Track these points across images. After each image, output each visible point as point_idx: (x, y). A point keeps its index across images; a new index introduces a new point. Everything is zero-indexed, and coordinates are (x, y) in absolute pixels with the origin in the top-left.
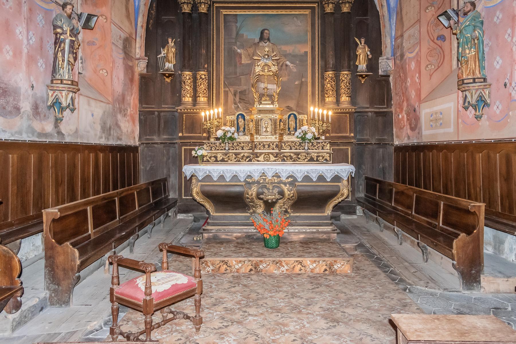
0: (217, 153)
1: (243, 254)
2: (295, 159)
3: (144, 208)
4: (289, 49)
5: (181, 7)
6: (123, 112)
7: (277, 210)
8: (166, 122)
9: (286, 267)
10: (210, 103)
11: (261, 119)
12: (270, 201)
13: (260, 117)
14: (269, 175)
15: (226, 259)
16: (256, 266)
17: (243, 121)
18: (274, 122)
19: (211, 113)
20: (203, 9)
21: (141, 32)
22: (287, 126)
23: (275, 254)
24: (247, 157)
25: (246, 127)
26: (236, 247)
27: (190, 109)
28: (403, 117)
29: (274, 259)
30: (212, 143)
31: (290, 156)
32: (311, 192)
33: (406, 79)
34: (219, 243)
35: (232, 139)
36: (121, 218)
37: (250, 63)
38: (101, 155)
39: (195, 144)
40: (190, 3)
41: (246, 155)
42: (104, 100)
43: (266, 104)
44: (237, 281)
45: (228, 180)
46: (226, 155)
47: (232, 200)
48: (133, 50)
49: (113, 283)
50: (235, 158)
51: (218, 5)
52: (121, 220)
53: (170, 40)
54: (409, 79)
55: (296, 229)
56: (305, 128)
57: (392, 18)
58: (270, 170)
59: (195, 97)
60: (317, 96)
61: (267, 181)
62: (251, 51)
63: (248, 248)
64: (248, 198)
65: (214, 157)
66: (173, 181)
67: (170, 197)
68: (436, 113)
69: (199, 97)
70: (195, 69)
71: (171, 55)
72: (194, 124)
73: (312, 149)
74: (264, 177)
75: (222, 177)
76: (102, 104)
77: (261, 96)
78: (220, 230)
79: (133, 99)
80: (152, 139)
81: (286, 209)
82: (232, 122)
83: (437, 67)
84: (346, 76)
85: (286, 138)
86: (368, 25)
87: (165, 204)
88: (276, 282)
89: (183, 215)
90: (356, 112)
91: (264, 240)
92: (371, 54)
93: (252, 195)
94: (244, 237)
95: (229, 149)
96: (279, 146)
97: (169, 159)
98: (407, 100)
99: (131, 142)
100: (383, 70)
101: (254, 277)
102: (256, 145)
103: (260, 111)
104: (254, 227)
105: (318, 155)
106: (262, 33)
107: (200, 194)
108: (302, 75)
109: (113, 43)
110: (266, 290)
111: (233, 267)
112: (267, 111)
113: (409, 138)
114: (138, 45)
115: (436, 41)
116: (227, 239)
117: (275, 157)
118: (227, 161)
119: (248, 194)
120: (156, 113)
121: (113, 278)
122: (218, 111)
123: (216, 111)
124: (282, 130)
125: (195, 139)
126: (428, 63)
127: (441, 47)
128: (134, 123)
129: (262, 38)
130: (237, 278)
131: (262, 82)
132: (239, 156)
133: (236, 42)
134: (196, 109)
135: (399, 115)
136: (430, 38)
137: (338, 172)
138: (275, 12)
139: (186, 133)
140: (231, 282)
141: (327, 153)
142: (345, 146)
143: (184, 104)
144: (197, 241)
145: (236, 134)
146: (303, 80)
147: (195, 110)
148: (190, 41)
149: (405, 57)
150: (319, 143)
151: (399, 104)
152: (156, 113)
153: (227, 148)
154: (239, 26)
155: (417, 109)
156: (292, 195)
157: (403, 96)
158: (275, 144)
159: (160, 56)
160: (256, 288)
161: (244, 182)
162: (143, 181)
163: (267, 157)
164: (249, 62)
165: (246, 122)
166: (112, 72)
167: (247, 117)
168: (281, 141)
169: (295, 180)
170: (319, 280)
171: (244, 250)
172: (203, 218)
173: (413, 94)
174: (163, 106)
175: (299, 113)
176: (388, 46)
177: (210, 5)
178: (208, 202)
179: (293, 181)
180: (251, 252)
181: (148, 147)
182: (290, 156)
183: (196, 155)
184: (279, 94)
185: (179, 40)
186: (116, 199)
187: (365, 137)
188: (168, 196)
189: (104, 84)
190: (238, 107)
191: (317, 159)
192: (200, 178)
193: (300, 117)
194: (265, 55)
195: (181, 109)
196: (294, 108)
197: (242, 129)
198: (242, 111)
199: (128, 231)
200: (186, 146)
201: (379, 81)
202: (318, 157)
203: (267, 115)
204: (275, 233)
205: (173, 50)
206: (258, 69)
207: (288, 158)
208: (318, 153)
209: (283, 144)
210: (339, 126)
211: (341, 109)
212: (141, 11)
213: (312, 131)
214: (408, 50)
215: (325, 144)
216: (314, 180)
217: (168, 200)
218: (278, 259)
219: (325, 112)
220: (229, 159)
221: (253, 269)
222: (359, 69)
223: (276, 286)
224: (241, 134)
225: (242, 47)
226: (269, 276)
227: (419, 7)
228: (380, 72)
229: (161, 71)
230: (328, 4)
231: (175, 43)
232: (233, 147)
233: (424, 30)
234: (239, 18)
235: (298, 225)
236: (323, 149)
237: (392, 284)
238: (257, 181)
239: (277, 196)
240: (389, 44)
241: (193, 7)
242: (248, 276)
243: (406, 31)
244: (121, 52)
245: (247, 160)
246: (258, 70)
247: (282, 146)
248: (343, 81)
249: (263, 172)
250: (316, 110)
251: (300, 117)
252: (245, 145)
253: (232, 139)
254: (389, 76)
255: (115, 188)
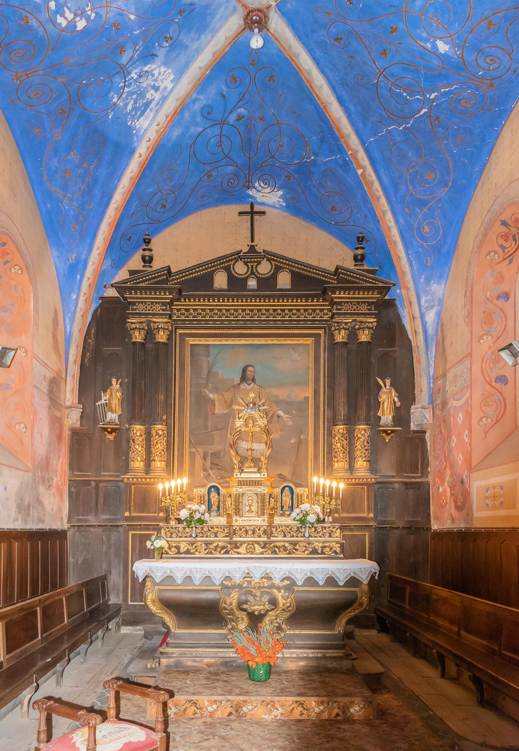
0: (179, 542)
1: (219, 691)
2: (290, 551)
3: (75, 620)
4: (282, 393)
5: (131, 335)
6: (47, 482)
7: (266, 625)
8: (107, 497)
9: (281, 710)
10: (169, 471)
11: (243, 494)
12: (256, 613)
13: (241, 490)
14: (257, 576)
15: (195, 698)
16: (238, 708)
17: (217, 496)
18: (262, 498)
19: (171, 485)
20: (161, 337)
21: (74, 369)
22: (279, 504)
23: (265, 690)
24: (223, 548)
25: (222, 505)
26: (208, 679)
27: (141, 478)
28: (445, 491)
29: (263, 698)
30: (172, 528)
31: (284, 546)
32: (316, 600)
33: (449, 436)
34: (183, 672)
35: (201, 521)
36: (44, 635)
37: (228, 413)
38: (16, 545)
39: (147, 527)
40: (143, 329)
41: (221, 544)
42: (20, 467)
43: (251, 472)
44: (211, 731)
45: (197, 583)
46: (192, 545)
47: (202, 612)
48: (62, 396)
49: (39, 741)
50: (205, 549)
51: (182, 331)
52: (43, 639)
53: (114, 381)
54: (454, 438)
55: (293, 653)
56: (305, 506)
57: (430, 349)
58: (258, 568)
59: (148, 461)
60: (321, 460)
61: (252, 584)
62: (228, 395)
63: (226, 681)
64: (225, 609)
65: (176, 547)
66: (115, 579)
67: (111, 602)
68: (494, 487)
69: (154, 460)
70: (149, 421)
71: (115, 403)
72: (146, 499)
73: (315, 537)
74: (248, 579)
75: (188, 579)
76: (19, 473)
77: (243, 460)
78: (185, 654)
79: (61, 463)
80: (86, 520)
81: (280, 625)
82: (201, 497)
83: (494, 421)
84: (363, 432)
85: (277, 520)
86: (395, 359)
87: (104, 613)
88: (266, 732)
89: (129, 627)
90: (377, 483)
91: (248, 668)
92: (399, 401)
93: (231, 604)
94: (218, 665)
95: (197, 536)
96: (268, 533)
97: (111, 548)
98: (452, 467)
99: (57, 525)
100: (416, 423)
101: (235, 725)
102: (235, 530)
103: (242, 483)
104: (234, 650)
105: (324, 544)
106: (244, 371)
107: (157, 603)
108: (301, 430)
109: (35, 386)
110: (253, 744)
111: (204, 710)
112: (251, 483)
113: (453, 520)
114: (68, 388)
115: (493, 384)
116: (194, 667)
117: (262, 548)
118: (193, 554)
119: (225, 603)
120: (93, 484)
121: (39, 732)
122: (180, 482)
123: (179, 482)
124: (273, 509)
125: (149, 521)
126: (482, 415)
127: (501, 393)
128: (61, 498)
129: (244, 378)
130: (211, 727)
131: (243, 440)
132: (211, 546)
133: (207, 384)
134: (150, 478)
135: (438, 488)
136: (486, 380)
137: (354, 573)
138: (262, 341)
139: (135, 511)
140: (203, 733)
141: (337, 542)
142: (361, 531)
143: (132, 471)
144: (151, 668)
145: (207, 515)
146: (302, 437)
147: (148, 480)
148: (143, 382)
149: (449, 406)
150: (325, 528)
151: (439, 472)
152: (93, 484)
153: (194, 535)
154: (211, 362)
155: (466, 480)
156: (288, 604)
157: (446, 461)
158: (262, 529)
159: (99, 403)
160: (239, 742)
161: (220, 585)
162: (73, 581)
163: (251, 548)
164: (226, 411)
165: (221, 498)
166: (32, 427)
167: (223, 491)
168: (271, 524)
169: (293, 583)
170: (329, 730)
171: (220, 683)
172: (159, 633)
173: (460, 459)
174: (103, 473)
175: (298, 485)
176: (423, 389)
177: (171, 332)
178: (168, 614)
179: (290, 584)
180: (229, 687)
181: (80, 532)
182: (284, 546)
183: (152, 547)
184: (268, 458)
185: (126, 380)
186: (38, 609)
187: (390, 519)
188: (107, 601)
189: (22, 443)
190: (209, 475)
191: (322, 550)
192: (158, 581)
193: (298, 490)
194: (250, 403)
195: (128, 479)
196: (289, 478)
197: (215, 507)
198: (215, 482)
199: (55, 655)
200: (135, 530)
201: (411, 438)
202: (323, 547)
203: (251, 488)
204: (264, 659)
205: (119, 394)
206: (239, 423)
207: (281, 549)
208: (323, 542)
209: (274, 530)
210: (353, 502)
211: (356, 479)
212: (73, 340)
213: (313, 510)
214: (453, 395)
215: (334, 530)
216: (321, 583)
217: (108, 606)
218: (269, 698)
219: (334, 484)
220: (197, 551)
221: (234, 713)
222: (382, 423)
223: (268, 739)
224: (213, 514)
225: (215, 390)
226: (256, 723)
227: (469, 335)
228: (413, 427)
229: (101, 425)
230: (339, 330)
231: (121, 384)
232: (202, 533)
233: (476, 368)
234: (213, 351)
235: (296, 648)
236: (330, 536)
237: (434, 737)
238: (239, 584)
239: (268, 607)
240: (426, 386)
241: (147, 334)
242: (226, 723)
243: (449, 369)
244: (46, 398)
245: (223, 552)
246: (239, 425)
247: (272, 533)
248: (359, 438)
249: (247, 571)
250: (322, 481)
251: (298, 490)
252: (219, 530)
253: (201, 521)
254: (424, 432)
255: (34, 593)
